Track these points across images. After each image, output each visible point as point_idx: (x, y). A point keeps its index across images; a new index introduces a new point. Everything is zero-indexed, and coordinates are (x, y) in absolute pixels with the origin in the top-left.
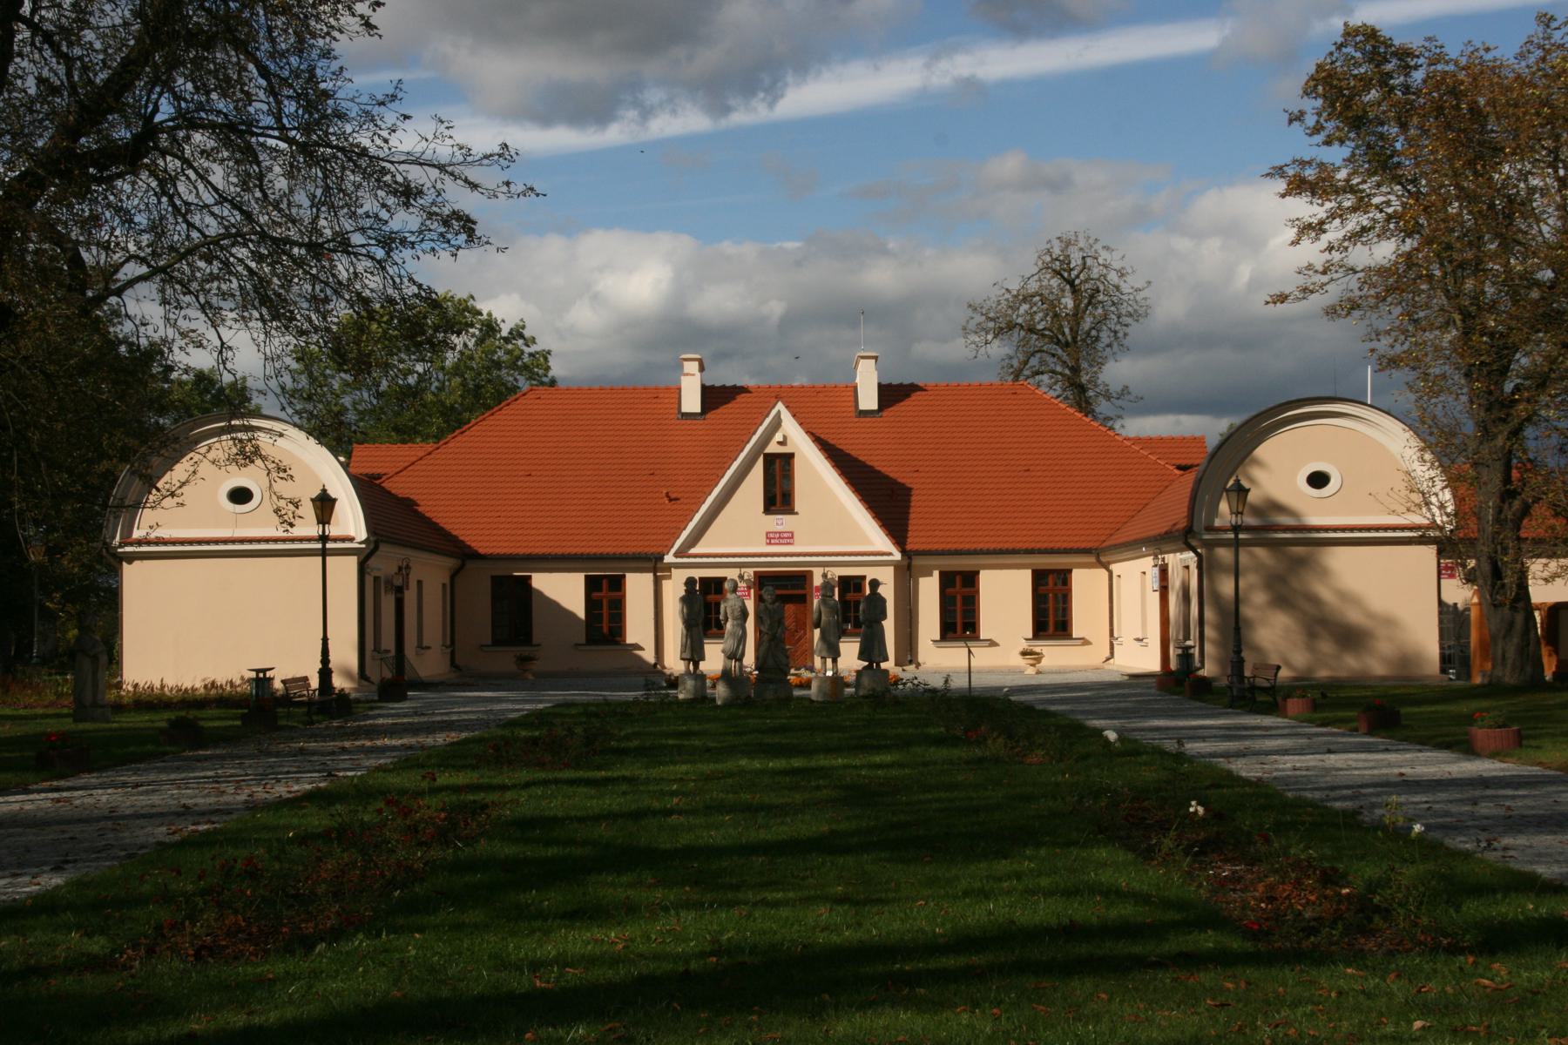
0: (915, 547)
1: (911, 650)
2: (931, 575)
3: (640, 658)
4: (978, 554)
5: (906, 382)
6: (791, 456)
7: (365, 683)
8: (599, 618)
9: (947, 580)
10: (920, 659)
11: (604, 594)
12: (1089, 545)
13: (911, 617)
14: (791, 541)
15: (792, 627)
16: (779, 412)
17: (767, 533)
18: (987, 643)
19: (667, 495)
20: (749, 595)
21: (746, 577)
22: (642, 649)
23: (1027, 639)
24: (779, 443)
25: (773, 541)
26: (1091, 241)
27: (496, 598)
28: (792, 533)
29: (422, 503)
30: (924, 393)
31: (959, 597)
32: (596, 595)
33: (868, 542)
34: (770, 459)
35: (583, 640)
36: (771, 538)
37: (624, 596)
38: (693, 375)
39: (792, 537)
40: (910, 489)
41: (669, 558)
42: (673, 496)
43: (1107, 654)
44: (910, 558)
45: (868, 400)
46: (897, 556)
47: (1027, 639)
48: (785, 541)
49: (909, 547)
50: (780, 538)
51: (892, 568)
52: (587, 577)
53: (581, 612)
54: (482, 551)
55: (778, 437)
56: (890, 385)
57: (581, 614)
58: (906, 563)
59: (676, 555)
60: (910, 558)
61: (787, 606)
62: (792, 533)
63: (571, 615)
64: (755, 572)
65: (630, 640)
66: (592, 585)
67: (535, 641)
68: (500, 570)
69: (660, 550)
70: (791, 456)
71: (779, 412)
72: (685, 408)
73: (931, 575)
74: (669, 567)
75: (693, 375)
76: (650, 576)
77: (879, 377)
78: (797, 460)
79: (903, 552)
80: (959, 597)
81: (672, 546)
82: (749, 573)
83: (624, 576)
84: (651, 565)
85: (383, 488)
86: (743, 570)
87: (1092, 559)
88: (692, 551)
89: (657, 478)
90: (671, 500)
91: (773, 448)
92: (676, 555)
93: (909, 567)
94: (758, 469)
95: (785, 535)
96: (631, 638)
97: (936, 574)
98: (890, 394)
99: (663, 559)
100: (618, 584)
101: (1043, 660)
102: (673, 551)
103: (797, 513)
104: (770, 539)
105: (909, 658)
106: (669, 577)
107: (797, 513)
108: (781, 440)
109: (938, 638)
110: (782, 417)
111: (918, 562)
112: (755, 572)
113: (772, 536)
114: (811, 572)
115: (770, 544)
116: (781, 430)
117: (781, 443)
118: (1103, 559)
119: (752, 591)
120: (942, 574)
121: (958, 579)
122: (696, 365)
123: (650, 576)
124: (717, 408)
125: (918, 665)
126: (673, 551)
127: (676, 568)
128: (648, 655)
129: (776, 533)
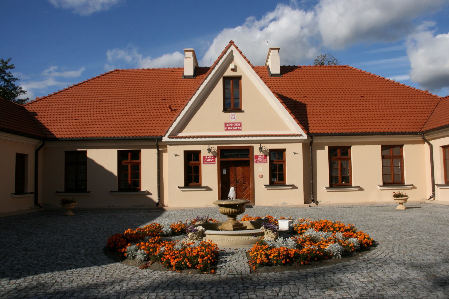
0: (315, 132)
1: (313, 193)
2: (324, 149)
3: (151, 200)
4: (353, 135)
5: (291, 65)
6: (239, 78)
7: (37, 207)
8: (126, 176)
9: (332, 151)
10: (318, 199)
11: (128, 162)
12: (415, 130)
13: (313, 174)
14: (240, 128)
15: (241, 180)
16: (232, 51)
17: (225, 124)
18: (357, 189)
19: (170, 107)
20: (215, 161)
21: (212, 150)
22: (151, 194)
23: (266, 186)
24: (232, 70)
25: (229, 128)
26: (331, 56)
27: (67, 164)
28: (241, 123)
29: (39, 114)
30: (301, 69)
31: (277, 174)
32: (124, 162)
33: (287, 128)
34: (226, 79)
35: (116, 189)
36: (227, 126)
37: (140, 163)
38: (190, 58)
39: (241, 126)
40: (305, 104)
41: (165, 139)
42: (173, 108)
43: (431, 194)
44: (312, 138)
45: (277, 71)
46: (305, 137)
47: (266, 186)
48: (236, 128)
49: (311, 132)
50: (233, 126)
51: (301, 145)
52: (119, 152)
53: (115, 171)
54: (58, 136)
55: (232, 66)
56: (284, 66)
57: (115, 172)
58: (309, 141)
59: (170, 137)
60: (312, 138)
61: (238, 168)
62: (241, 123)
63: (111, 174)
64: (218, 147)
65: (144, 188)
66: (121, 156)
67: (88, 190)
68: (70, 147)
69: (160, 134)
70: (239, 78)
71: (232, 51)
72: (186, 74)
73: (324, 149)
74: (166, 145)
75: (190, 58)
76: (155, 151)
77: (281, 60)
78: (243, 81)
79: (308, 134)
80: (277, 174)
81: (167, 132)
82: (214, 147)
83: (140, 151)
84: (155, 143)
85: (24, 108)
86: (211, 146)
87: (420, 139)
88: (180, 135)
89: (166, 101)
90: (172, 110)
91: (229, 73)
92: (170, 137)
93: (311, 143)
94: (220, 85)
95: (236, 125)
96: (144, 188)
97: (326, 148)
98: (285, 70)
99: (162, 139)
100: (137, 155)
101: (408, 200)
102: (168, 134)
103: (243, 112)
104: (227, 127)
105: (312, 199)
106: (166, 151)
107: (243, 112)
108: (233, 68)
109: (183, 185)
110: (234, 54)
111: (317, 140)
112: (218, 147)
113: (228, 125)
114: (252, 147)
115: (227, 130)
116: (233, 62)
117: (233, 70)
118: (427, 138)
119: (216, 158)
120: (329, 148)
121: (338, 151)
122: (191, 53)
123: (155, 151)
124: (202, 74)
125: (317, 203)
126: (168, 134)
127: (170, 145)
128: (155, 197)
129: (230, 123)
